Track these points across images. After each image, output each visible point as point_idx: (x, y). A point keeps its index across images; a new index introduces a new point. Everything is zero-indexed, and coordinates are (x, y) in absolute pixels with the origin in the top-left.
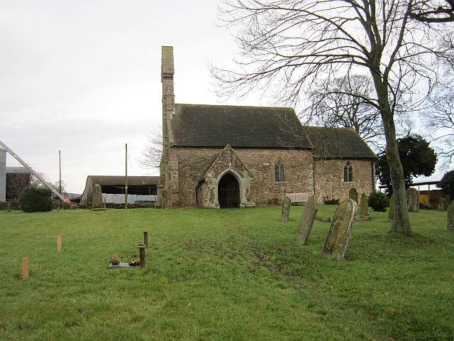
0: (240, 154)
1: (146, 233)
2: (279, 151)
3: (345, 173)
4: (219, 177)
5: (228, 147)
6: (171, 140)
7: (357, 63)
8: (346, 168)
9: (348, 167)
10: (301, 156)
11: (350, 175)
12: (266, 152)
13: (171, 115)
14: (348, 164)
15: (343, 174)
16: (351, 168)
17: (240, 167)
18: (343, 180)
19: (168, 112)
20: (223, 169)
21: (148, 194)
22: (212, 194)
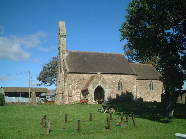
0: (106, 77)
1: (79, 121)
2: (120, 75)
3: (150, 86)
4: (95, 88)
5: (99, 73)
6: (68, 69)
7: (62, 37)
8: (150, 84)
9: (120, 83)
10: (131, 77)
11: (152, 87)
12: (114, 76)
13: (65, 56)
14: (151, 82)
15: (149, 87)
16: (152, 84)
17: (105, 83)
18: (149, 90)
19: (64, 54)
20: (96, 84)
21: (20, 97)
22: (91, 97)
